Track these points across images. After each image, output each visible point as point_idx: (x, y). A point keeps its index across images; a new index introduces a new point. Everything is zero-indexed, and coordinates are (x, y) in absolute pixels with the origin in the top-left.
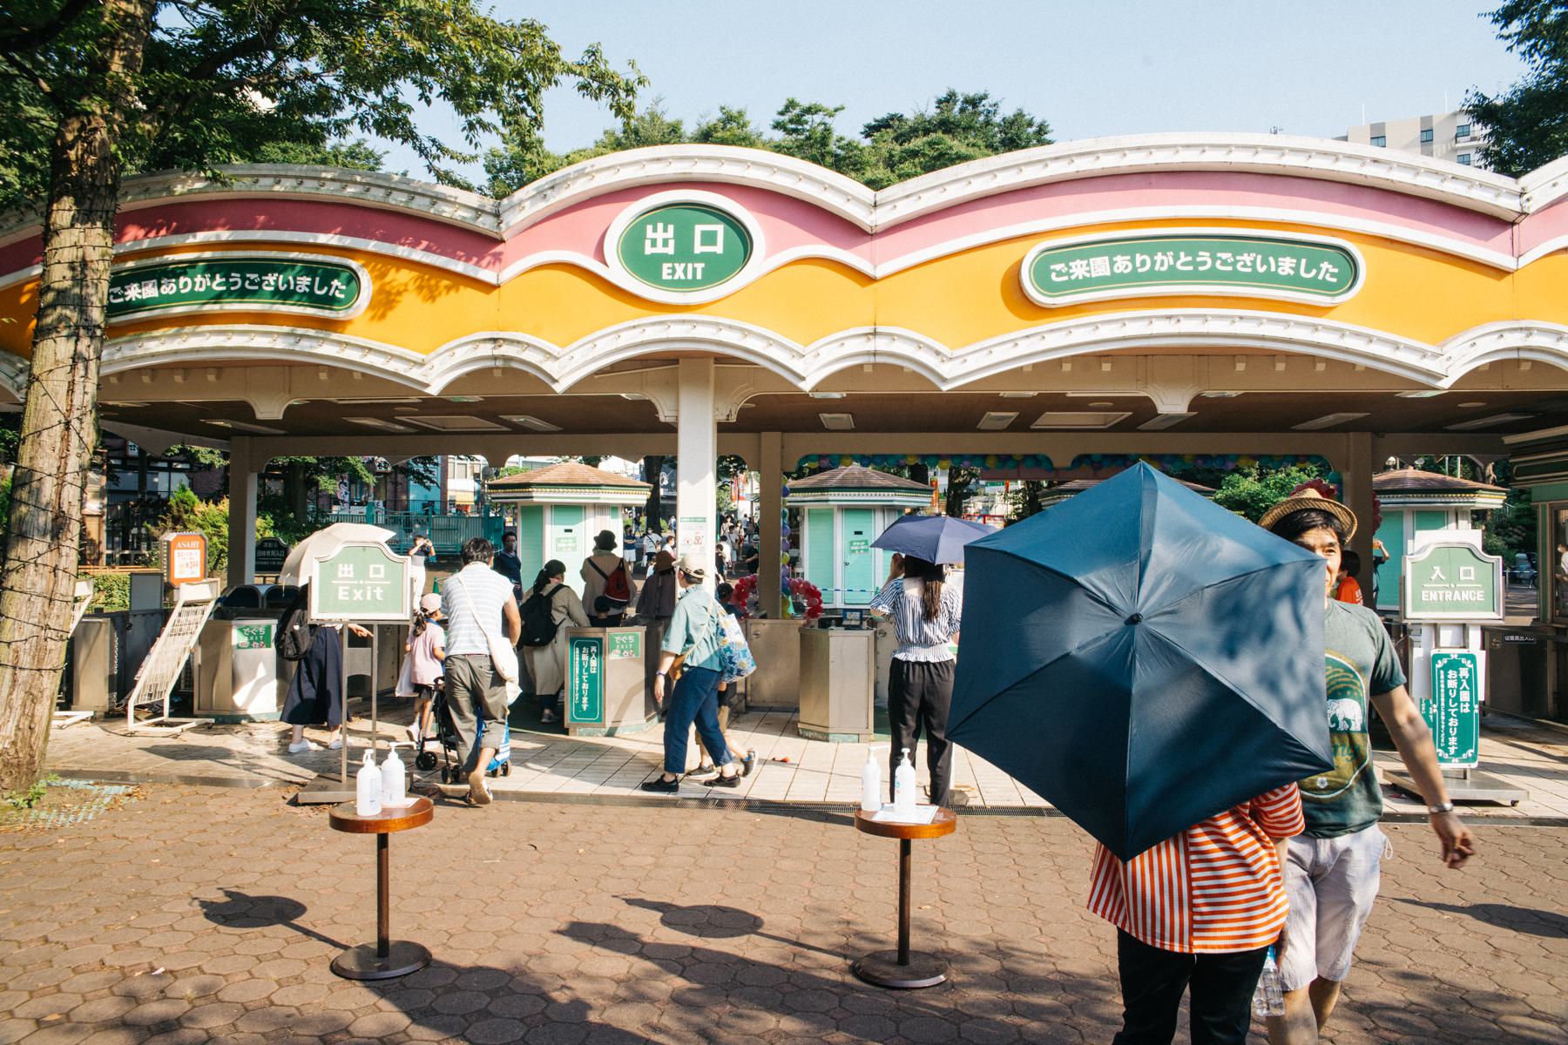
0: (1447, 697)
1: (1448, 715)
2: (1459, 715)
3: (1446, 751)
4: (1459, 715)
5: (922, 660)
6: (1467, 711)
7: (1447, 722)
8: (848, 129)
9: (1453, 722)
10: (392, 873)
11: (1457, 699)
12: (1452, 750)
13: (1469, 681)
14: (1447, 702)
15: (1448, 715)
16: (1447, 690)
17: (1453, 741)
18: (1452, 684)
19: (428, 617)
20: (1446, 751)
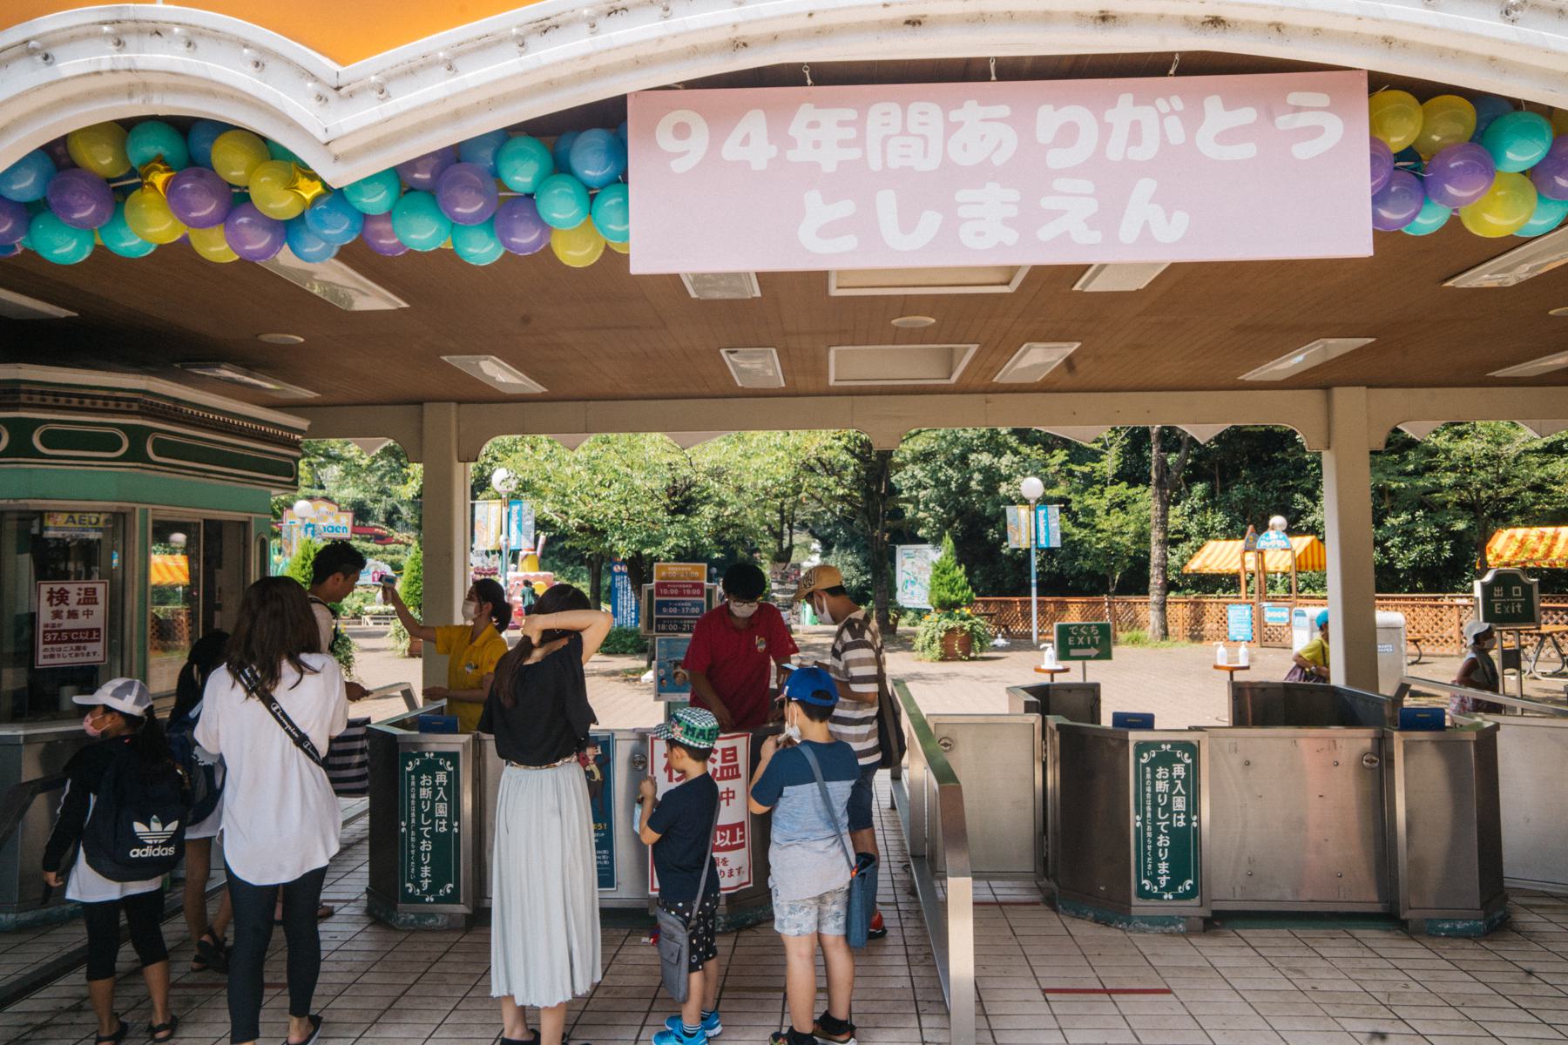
0: (419, 811)
1: (1157, 831)
2: (434, 836)
3: (1156, 882)
4: (434, 836)
5: (886, 923)
6: (1182, 824)
7: (1155, 840)
8: (1382, 447)
9: (1163, 841)
10: (807, 399)
11: (1168, 808)
12: (1163, 880)
13: (447, 790)
14: (1154, 813)
15: (420, 837)
16: (418, 801)
17: (426, 871)
18: (425, 793)
19: (1317, 533)
20: (1156, 882)
